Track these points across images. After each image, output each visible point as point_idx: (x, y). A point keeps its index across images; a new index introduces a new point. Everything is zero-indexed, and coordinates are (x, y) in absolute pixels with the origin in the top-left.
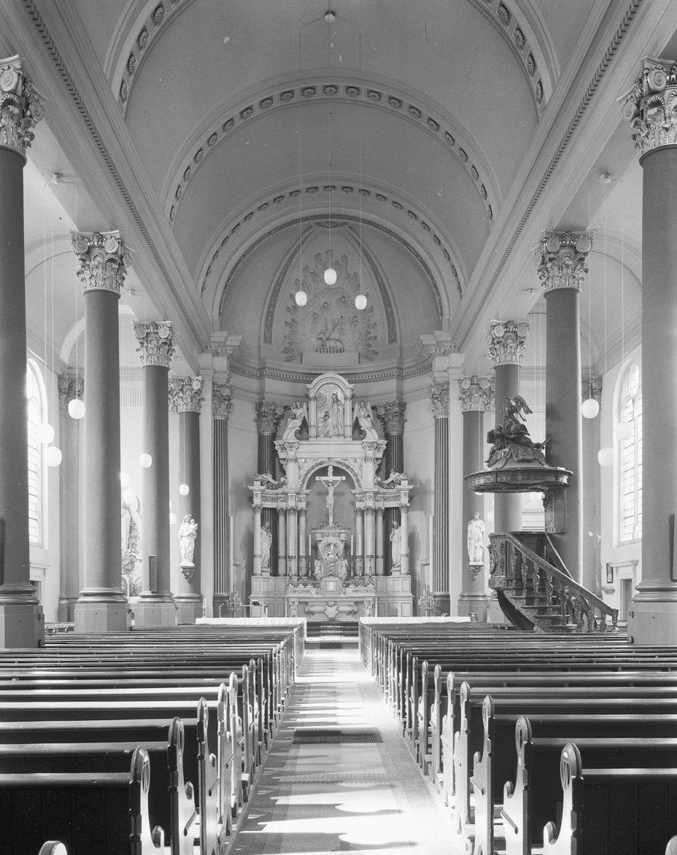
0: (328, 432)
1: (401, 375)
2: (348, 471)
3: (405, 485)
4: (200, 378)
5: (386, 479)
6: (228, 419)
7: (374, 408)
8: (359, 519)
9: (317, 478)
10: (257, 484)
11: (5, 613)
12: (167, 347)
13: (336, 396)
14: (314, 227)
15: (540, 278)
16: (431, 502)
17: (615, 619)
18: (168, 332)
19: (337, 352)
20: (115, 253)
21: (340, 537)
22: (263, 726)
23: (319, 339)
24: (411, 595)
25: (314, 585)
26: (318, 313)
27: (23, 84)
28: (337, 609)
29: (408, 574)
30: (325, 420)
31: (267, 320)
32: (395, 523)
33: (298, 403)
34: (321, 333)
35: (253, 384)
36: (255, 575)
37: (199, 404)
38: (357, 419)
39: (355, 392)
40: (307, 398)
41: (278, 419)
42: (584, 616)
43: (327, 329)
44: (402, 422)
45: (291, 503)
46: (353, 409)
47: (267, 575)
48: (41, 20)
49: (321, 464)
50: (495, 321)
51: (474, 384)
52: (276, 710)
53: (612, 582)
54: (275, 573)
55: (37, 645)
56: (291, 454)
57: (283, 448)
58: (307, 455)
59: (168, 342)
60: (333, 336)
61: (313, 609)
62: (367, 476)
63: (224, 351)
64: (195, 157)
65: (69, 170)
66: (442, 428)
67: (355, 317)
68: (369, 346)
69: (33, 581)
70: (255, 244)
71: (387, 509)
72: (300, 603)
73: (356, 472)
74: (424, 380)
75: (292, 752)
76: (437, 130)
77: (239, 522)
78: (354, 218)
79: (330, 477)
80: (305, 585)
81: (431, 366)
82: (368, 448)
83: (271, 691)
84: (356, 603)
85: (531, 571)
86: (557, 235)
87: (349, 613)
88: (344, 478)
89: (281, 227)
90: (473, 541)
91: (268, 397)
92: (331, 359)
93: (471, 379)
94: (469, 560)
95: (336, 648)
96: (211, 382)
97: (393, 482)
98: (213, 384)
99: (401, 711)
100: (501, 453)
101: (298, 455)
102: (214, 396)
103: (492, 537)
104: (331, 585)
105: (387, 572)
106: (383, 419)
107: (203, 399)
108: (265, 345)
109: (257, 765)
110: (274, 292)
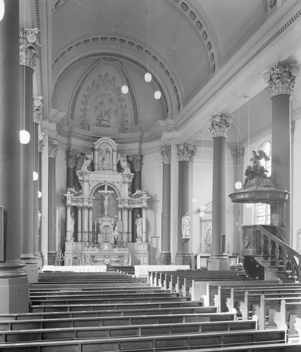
0: (104, 168)
1: (141, 141)
2: (114, 188)
3: (145, 196)
4: (43, 134)
6: (56, 157)
7: (127, 156)
8: (120, 213)
9: (99, 191)
10: (69, 193)
11: (9, 285)
13: (109, 149)
14: (102, 60)
16: (159, 206)
18: (40, 103)
20: (34, 43)
21: (111, 222)
23: (97, 119)
24: (148, 252)
25: (98, 247)
29: (146, 242)
30: (103, 162)
31: (72, 107)
32: (139, 216)
33: (89, 151)
34: (98, 117)
36: (67, 241)
37: (41, 148)
38: (119, 161)
40: (93, 150)
41: (77, 159)
43: (102, 115)
44: (141, 164)
45: (86, 204)
46: (117, 157)
47: (72, 241)
49: (101, 184)
50: (216, 113)
51: (185, 147)
54: (76, 240)
56: (86, 178)
57: (81, 174)
58: (93, 179)
60: (105, 119)
61: (98, 259)
62: (125, 191)
63: (55, 120)
64: (56, 5)
66: (167, 168)
68: (123, 125)
70: (72, 64)
71: (134, 208)
72: (91, 256)
73: (118, 189)
74: (156, 144)
77: (59, 212)
78: (123, 57)
79: (106, 191)
80: (93, 247)
81: (161, 136)
82: (125, 177)
85: (274, 247)
86: (283, 65)
87: (116, 262)
88: (113, 192)
89: (86, 57)
90: (185, 226)
91: (73, 147)
92: (103, 130)
93: (184, 145)
94: (182, 236)
96: (48, 137)
97: (137, 195)
98: (49, 138)
100: (254, 181)
101: (90, 179)
102: (49, 144)
104: (106, 247)
105: (134, 241)
106: (131, 162)
107: (44, 145)
110: (76, 92)
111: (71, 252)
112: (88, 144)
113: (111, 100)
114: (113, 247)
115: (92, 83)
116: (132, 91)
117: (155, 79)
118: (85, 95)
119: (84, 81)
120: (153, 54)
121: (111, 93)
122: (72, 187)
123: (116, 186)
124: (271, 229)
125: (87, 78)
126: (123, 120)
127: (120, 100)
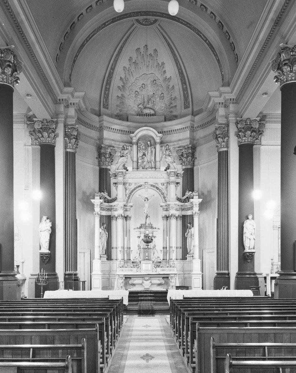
10: (97, 198)
26: (139, 91)
30: (143, 158)
31: (105, 93)
35: (94, 134)
39: (162, 139)
43: (144, 102)
48: (10, 7)
52: (117, 333)
60: (148, 106)
61: (135, 282)
67: (162, 93)
68: (171, 112)
72: (126, 278)
84: (163, 278)
87: (159, 285)
94: (244, 249)
95: (150, 314)
97: (187, 198)
99: (173, 326)
101: (125, 181)
105: (184, 258)
108: (104, 109)
110: (109, 74)
111: (101, 273)
112: (125, 137)
113: (155, 82)
114: (156, 266)
115: (129, 61)
116: (180, 64)
117: (206, 38)
118: (121, 78)
119: (118, 59)
120: (232, 39)
121: (154, 73)
122: (104, 192)
123: (160, 188)
125: (121, 55)
127: (165, 79)
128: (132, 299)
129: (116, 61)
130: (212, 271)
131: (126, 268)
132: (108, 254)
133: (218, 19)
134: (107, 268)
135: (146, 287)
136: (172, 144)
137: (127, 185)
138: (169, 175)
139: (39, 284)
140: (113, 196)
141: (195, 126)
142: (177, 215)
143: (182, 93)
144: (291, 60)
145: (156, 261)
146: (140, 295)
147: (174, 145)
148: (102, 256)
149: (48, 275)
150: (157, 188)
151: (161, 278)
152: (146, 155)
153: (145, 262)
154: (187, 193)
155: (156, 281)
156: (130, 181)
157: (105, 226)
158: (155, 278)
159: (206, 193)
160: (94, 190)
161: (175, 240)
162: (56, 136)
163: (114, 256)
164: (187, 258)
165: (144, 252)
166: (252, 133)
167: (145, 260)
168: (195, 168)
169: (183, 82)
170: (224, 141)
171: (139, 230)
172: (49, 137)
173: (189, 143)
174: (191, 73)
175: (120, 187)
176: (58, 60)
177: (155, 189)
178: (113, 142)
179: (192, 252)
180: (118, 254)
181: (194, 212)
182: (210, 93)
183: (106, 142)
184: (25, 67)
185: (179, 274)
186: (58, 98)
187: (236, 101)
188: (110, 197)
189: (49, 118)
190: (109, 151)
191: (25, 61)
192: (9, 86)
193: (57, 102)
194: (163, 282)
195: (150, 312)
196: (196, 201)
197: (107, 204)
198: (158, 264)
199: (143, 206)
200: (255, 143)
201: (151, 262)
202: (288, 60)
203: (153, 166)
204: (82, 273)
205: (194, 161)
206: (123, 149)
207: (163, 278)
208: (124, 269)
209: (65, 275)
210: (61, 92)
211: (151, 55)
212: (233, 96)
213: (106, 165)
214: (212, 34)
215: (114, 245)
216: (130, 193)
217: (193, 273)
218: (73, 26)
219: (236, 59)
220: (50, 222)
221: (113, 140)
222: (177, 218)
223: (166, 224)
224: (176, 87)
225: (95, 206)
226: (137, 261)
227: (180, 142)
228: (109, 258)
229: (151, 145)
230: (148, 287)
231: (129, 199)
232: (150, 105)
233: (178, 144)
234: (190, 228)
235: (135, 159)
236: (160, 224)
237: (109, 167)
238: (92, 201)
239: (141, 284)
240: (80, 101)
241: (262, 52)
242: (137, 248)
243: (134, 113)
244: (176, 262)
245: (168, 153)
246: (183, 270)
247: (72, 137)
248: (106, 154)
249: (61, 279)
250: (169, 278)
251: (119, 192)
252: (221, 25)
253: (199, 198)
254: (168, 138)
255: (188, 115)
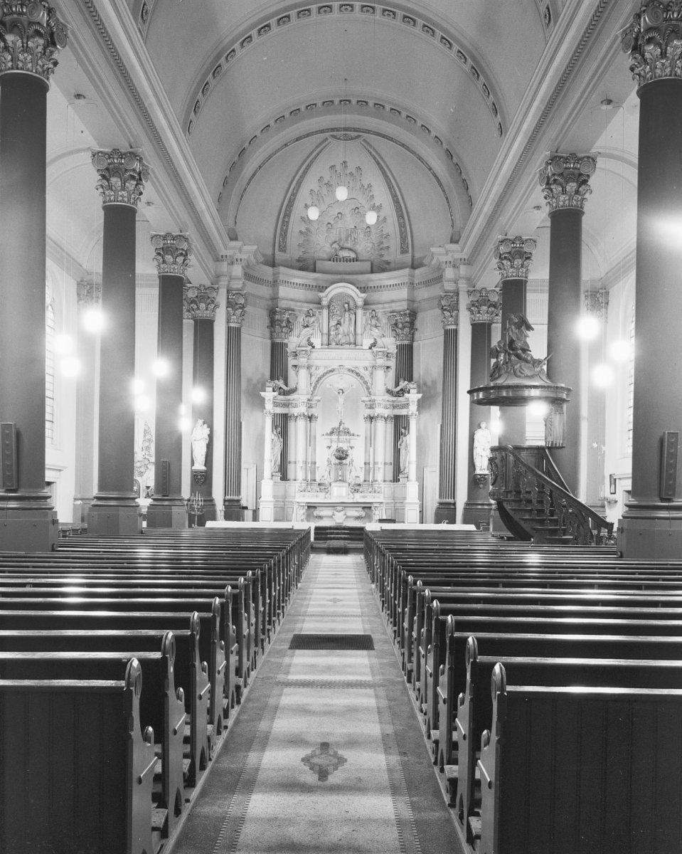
5: (396, 387)
12: (182, 258)
13: (348, 303)
14: (330, 140)
15: (545, 198)
17: (610, 531)
19: (350, 261)
22: (259, 631)
26: (332, 222)
27: (48, 15)
28: (345, 514)
30: (337, 329)
31: (282, 229)
35: (265, 291)
42: (581, 527)
53: (615, 493)
55: (50, 549)
59: (184, 253)
61: (322, 514)
65: (89, 90)
66: (451, 339)
68: (382, 256)
69: (48, 482)
72: (308, 507)
75: (287, 660)
76: (450, 48)
78: (368, 132)
83: (270, 598)
84: (364, 508)
87: (358, 518)
94: (475, 469)
95: (342, 553)
97: (402, 390)
99: (392, 620)
101: (311, 362)
103: (493, 450)
105: (396, 480)
109: (252, 670)
110: (289, 202)
112: (310, 295)
114: (353, 491)
124: (206, 472)
126: (382, 246)
128: (320, 536)
129: (299, 184)
130: (433, 499)
131: (310, 493)
132: (283, 471)
133: (445, 146)
134: (281, 493)
135: (338, 521)
136: (381, 306)
137: (313, 368)
138: (375, 355)
139: (193, 513)
140: (292, 385)
141: (416, 281)
142: (386, 416)
143: (397, 229)
144: (512, 252)
145: (353, 483)
146: (328, 531)
147: (384, 308)
148: (274, 474)
149: (205, 501)
150: (358, 374)
151: (361, 509)
152: (342, 323)
153: (338, 483)
154: (400, 383)
155: (353, 512)
156: (317, 363)
157: (279, 429)
158: (351, 509)
159: (429, 383)
160: (263, 375)
161: (383, 452)
162: (217, 306)
163: (291, 475)
164: (401, 479)
165: (336, 470)
166: (489, 308)
167: (337, 481)
168: (415, 344)
169: (400, 215)
170: (452, 316)
171: (329, 437)
172: (207, 309)
173: (406, 307)
174: (412, 204)
175: (303, 373)
176: (221, 199)
177: (355, 375)
178: (292, 303)
179: (406, 471)
180: (297, 471)
181: (410, 413)
182: (433, 250)
183: (283, 304)
184: (154, 173)
185: (387, 503)
186: (221, 254)
187: (469, 262)
188: (286, 385)
189: (208, 283)
190: (286, 316)
191: (197, 243)
192: (131, 207)
193: (218, 259)
194: (363, 514)
195: (344, 551)
196: (414, 396)
197: (282, 397)
198: (356, 488)
199: (337, 400)
200: (495, 321)
201: (347, 485)
202: (510, 253)
203: (352, 341)
204: (246, 498)
205: (413, 334)
206: (308, 315)
207: (364, 508)
208: (307, 493)
209: (225, 501)
210: (226, 248)
211: (351, 174)
212: (464, 255)
213: (281, 338)
214: (439, 165)
215: (291, 457)
216: (318, 381)
217: (407, 501)
218: (242, 152)
219: (470, 203)
220: (208, 427)
221: (292, 300)
222: (386, 419)
223: (369, 428)
224: (390, 220)
225: (266, 402)
226: (326, 482)
227: (393, 304)
228: (284, 477)
229: (350, 309)
230: (341, 521)
231: (314, 389)
232: (349, 245)
233: (390, 307)
234: (405, 436)
235: (325, 331)
236: (360, 427)
237: (286, 341)
238: (263, 394)
239: (332, 517)
240: (249, 256)
241: (592, 29)
242: (327, 463)
243: (325, 256)
244: (383, 485)
245: (374, 322)
246: (394, 496)
247: (237, 306)
248: (282, 321)
249: (220, 507)
250: (373, 508)
251: (300, 379)
252: (449, 155)
253: (417, 393)
254: (376, 296)
255: (406, 268)
